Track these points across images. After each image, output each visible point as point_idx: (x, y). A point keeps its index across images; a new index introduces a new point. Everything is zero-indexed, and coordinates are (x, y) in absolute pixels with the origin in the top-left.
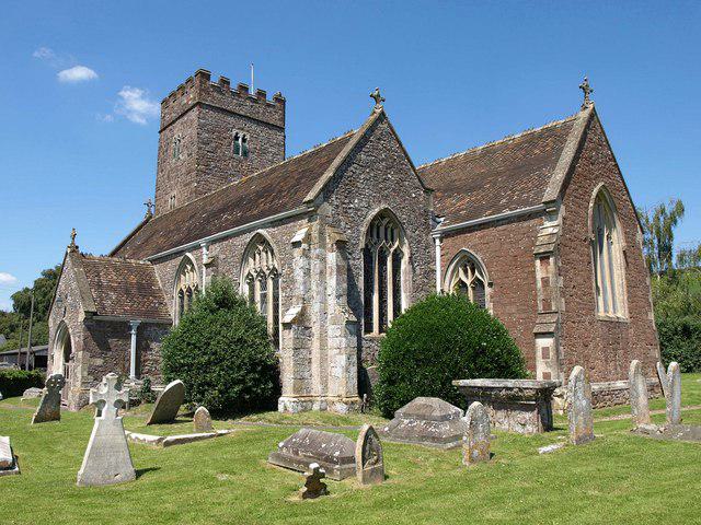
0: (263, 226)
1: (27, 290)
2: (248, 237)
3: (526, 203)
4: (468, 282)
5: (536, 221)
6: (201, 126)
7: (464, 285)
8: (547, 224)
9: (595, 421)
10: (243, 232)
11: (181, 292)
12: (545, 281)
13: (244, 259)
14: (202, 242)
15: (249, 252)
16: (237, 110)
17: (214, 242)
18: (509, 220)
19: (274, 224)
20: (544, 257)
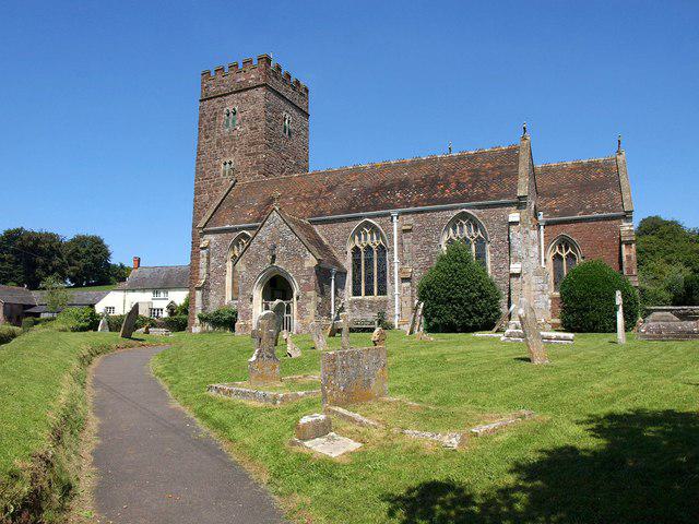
0: (369, 217)
1: (107, 255)
2: (455, 213)
3: (607, 210)
4: (564, 255)
5: (617, 222)
6: (267, 106)
7: (560, 258)
8: (624, 224)
9: (179, 297)
10: (452, 209)
11: (356, 250)
12: (629, 258)
13: (232, 247)
14: (395, 213)
15: (454, 223)
16: (285, 94)
17: (404, 213)
18: (597, 219)
19: (479, 207)
20: (628, 244)
